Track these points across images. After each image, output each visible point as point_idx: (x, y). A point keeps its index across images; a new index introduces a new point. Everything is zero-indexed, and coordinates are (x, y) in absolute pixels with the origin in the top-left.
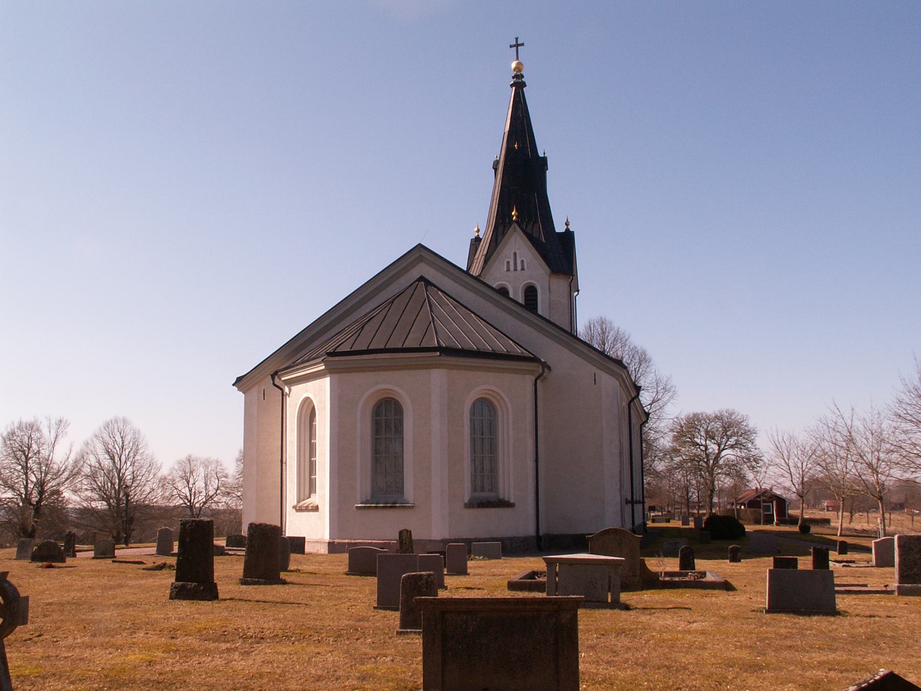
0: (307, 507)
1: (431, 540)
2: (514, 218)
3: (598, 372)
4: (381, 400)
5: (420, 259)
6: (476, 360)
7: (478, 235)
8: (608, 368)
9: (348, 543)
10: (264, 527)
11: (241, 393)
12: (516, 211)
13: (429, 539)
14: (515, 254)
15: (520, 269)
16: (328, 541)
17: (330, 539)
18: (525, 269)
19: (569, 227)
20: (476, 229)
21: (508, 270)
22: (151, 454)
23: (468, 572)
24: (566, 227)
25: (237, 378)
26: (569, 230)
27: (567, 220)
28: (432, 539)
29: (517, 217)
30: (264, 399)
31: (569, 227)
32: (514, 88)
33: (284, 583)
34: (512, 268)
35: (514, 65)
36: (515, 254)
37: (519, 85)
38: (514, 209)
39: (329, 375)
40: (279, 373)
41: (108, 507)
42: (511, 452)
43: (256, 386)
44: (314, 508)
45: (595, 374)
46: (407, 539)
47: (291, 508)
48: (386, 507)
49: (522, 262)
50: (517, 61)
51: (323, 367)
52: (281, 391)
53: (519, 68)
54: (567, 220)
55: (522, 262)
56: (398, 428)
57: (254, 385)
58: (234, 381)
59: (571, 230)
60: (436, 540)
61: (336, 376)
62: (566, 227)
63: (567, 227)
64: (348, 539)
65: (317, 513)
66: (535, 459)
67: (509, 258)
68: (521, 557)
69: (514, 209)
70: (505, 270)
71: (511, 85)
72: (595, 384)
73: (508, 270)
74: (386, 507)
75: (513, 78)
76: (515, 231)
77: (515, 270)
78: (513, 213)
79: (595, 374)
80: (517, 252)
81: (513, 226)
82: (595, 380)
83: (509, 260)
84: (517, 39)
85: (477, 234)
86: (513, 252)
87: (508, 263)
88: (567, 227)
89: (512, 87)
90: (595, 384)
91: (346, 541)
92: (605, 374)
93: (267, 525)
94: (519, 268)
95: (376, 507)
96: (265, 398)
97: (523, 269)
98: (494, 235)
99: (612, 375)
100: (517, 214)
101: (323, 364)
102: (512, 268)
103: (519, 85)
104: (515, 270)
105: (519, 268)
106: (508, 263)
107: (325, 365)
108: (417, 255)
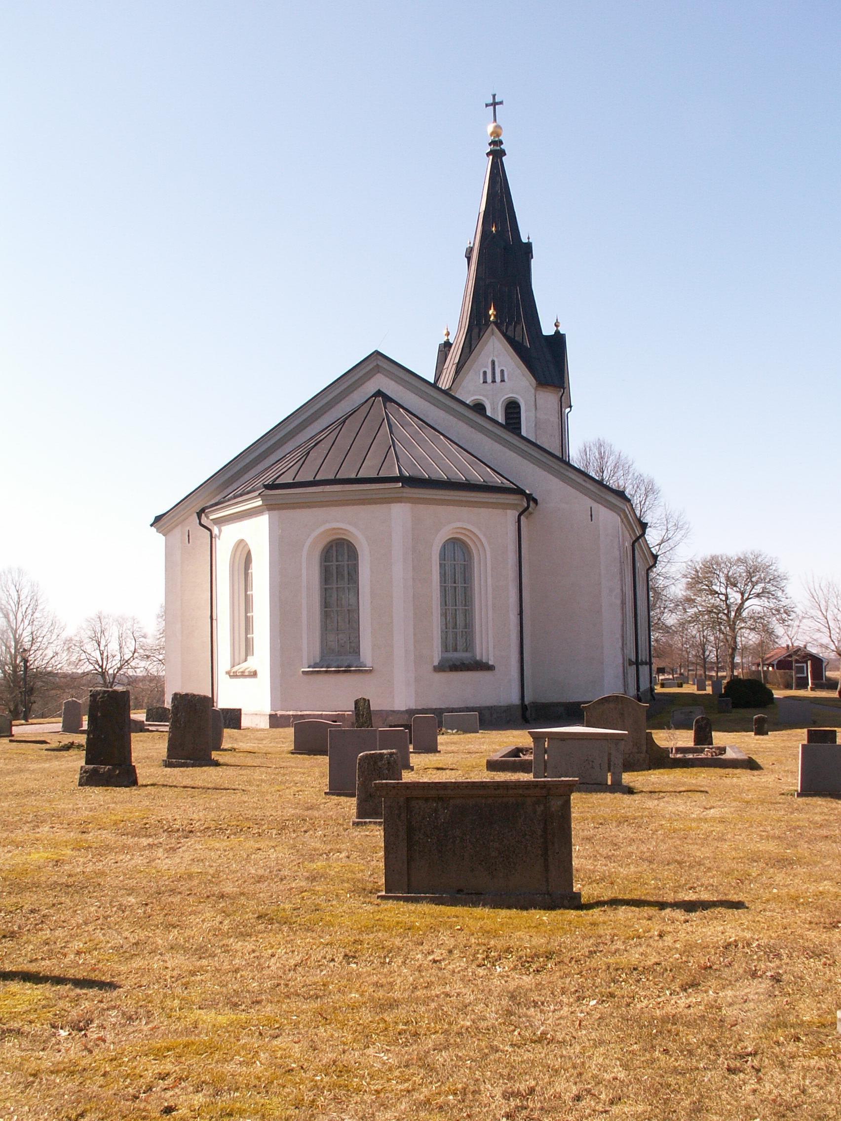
1: (394, 711)
3: (595, 506)
5: (377, 369)
6: (473, 494)
12: (494, 309)
14: (493, 363)
19: (559, 328)
20: (445, 332)
21: (485, 382)
24: (555, 328)
28: (395, 709)
31: (559, 328)
32: (491, 157)
34: (489, 379)
35: (490, 128)
36: (493, 363)
37: (497, 154)
42: (490, 603)
43: (179, 527)
49: (502, 371)
50: (495, 124)
51: (260, 503)
53: (496, 133)
55: (502, 371)
57: (177, 525)
61: (275, 513)
73: (485, 382)
75: (490, 144)
77: (494, 381)
78: (491, 312)
80: (495, 359)
82: (591, 516)
84: (494, 96)
87: (485, 373)
91: (291, 713)
92: (604, 508)
94: (498, 379)
95: (326, 672)
97: (503, 381)
102: (489, 379)
103: (497, 154)
104: (494, 381)
105: (498, 379)
106: (485, 373)
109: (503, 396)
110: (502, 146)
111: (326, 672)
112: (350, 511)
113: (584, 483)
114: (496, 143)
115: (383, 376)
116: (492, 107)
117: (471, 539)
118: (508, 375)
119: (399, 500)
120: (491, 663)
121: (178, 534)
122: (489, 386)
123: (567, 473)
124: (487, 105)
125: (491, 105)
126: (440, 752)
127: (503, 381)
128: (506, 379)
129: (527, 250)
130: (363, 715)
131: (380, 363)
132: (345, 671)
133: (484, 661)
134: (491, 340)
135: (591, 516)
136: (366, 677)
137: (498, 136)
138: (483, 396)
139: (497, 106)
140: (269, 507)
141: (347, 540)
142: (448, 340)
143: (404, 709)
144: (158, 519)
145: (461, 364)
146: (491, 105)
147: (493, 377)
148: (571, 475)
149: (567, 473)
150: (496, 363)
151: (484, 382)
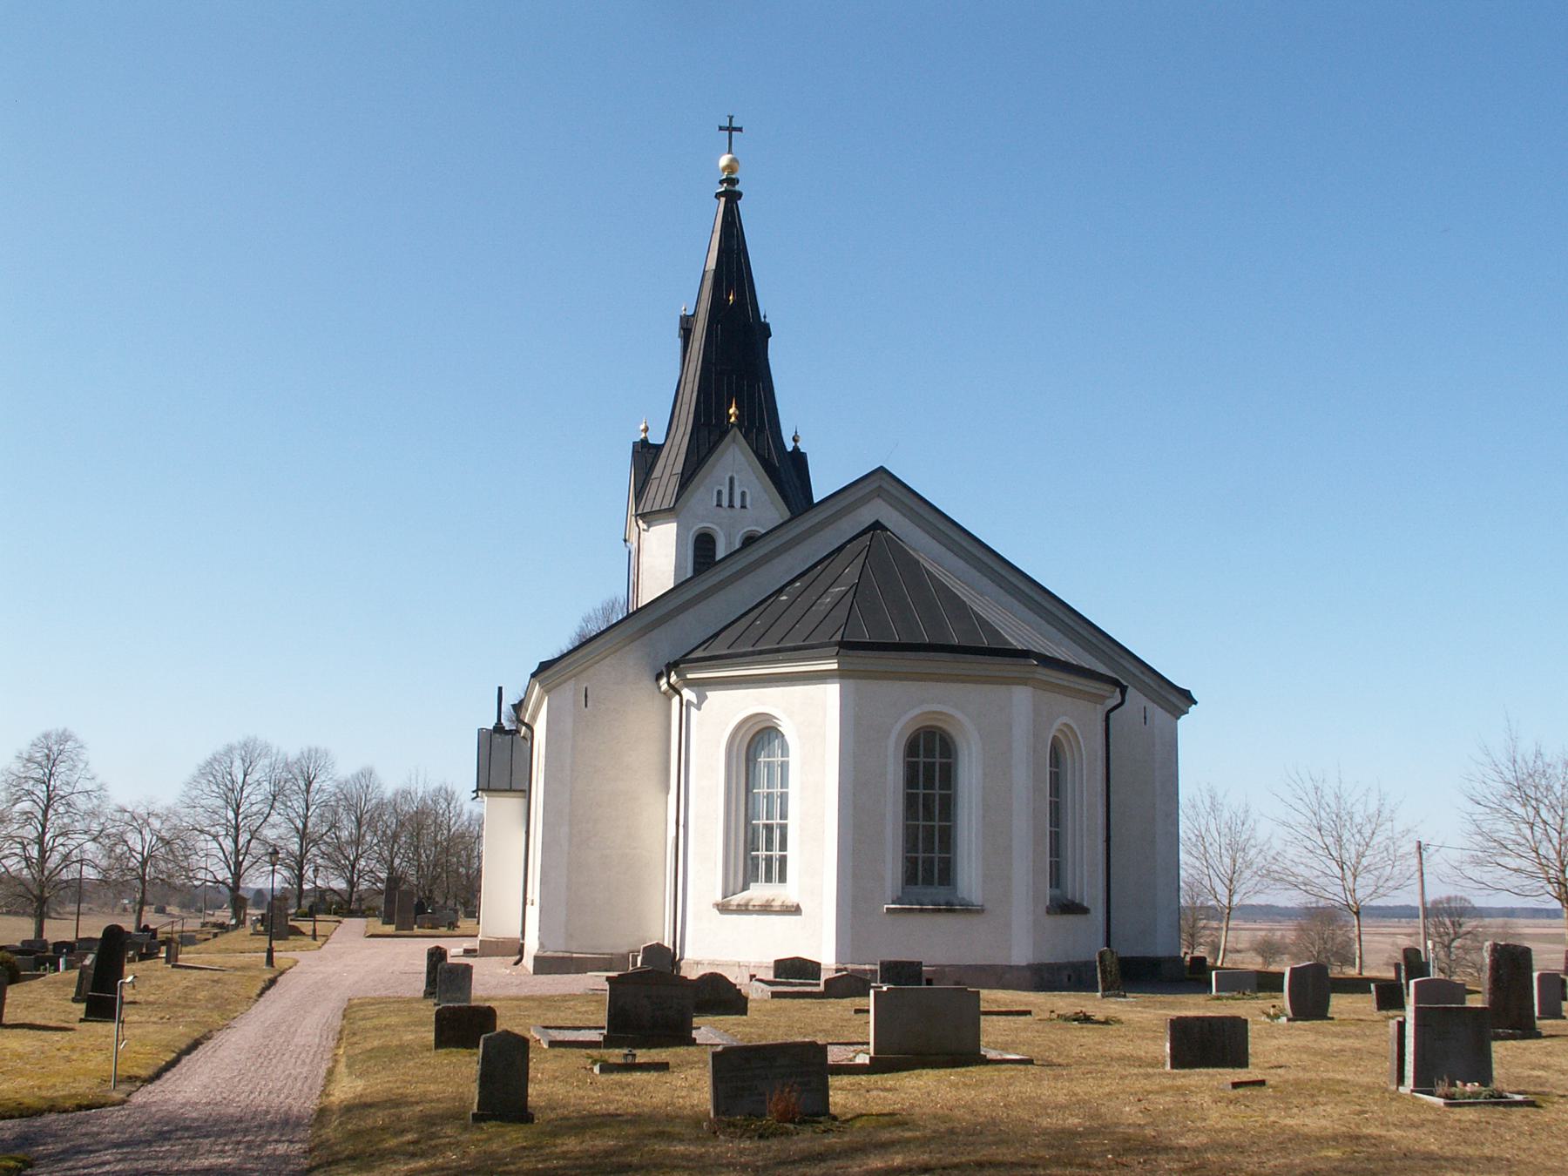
0: (747, 905)
1: (1011, 967)
2: (733, 419)
3: (1151, 706)
4: (921, 728)
5: (879, 492)
6: (1077, 679)
7: (646, 437)
8: (1168, 700)
9: (870, 970)
10: (1513, 949)
11: (1183, 717)
12: (736, 407)
13: (1008, 964)
14: (732, 480)
15: (727, 505)
16: (834, 967)
17: (836, 963)
18: (748, 506)
19: (798, 444)
20: (642, 427)
21: (719, 505)
22: (462, 801)
23: (1329, 1015)
24: (794, 444)
25: (541, 663)
26: (799, 450)
27: (796, 432)
28: (1012, 964)
29: (737, 417)
30: (586, 706)
31: (798, 444)
32: (723, 199)
33: (1539, 1036)
34: (725, 503)
35: (724, 160)
36: (732, 480)
37: (731, 197)
38: (734, 405)
39: (838, 680)
40: (681, 666)
41: (1199, 905)
43: (572, 682)
44: (793, 909)
45: (1145, 708)
46: (1113, 965)
47: (1092, 911)
48: (940, 910)
49: (743, 494)
50: (730, 156)
51: (835, 666)
52: (1111, 714)
53: (731, 167)
54: (796, 432)
55: (743, 494)
56: (948, 776)
57: (570, 678)
58: (534, 669)
59: (802, 451)
60: (1018, 966)
62: (794, 444)
63: (796, 445)
64: (869, 964)
65: (798, 917)
66: (1105, 839)
67: (721, 485)
68: (1152, 993)
69: (734, 405)
70: (715, 504)
71: (717, 193)
72: (1145, 723)
73: (719, 505)
74: (940, 910)
75: (721, 182)
76: (734, 441)
77: (731, 506)
78: (731, 411)
79: (1145, 708)
80: (736, 477)
81: (732, 433)
82: (1145, 718)
83: (721, 488)
84: (731, 118)
85: (643, 435)
86: (730, 474)
87: (719, 493)
88: (796, 445)
89: (719, 199)
90: (1145, 723)
91: (867, 967)
92: (1160, 709)
93: (1516, 946)
94: (737, 503)
95: (921, 910)
96: (588, 705)
97: (743, 507)
98: (692, 442)
99: (1169, 712)
100: (737, 412)
101: (836, 661)
102: (725, 503)
103: (731, 197)
104: (731, 506)
105: (737, 503)
106: (719, 493)
107: (838, 663)
108: (876, 485)
109: (743, 528)
110: (737, 187)
111: (921, 910)
112: (956, 689)
113: (1140, 675)
114: (731, 181)
115: (883, 503)
116: (727, 132)
117: (1069, 741)
118: (752, 499)
119: (1023, 681)
120: (1085, 904)
121: (569, 691)
122: (724, 512)
123: (1121, 661)
124: (721, 128)
125: (727, 129)
126: (1332, 1019)
127: (743, 507)
128: (748, 504)
129: (765, 331)
130: (1111, 971)
131: (885, 486)
132: (948, 911)
133: (1077, 901)
134: (731, 449)
135: (1145, 718)
136: (974, 920)
137: (732, 172)
138: (717, 525)
139: (734, 133)
140: (839, 675)
141: (940, 728)
142: (646, 437)
143: (1024, 963)
144: (544, 667)
145: (686, 476)
146: (727, 129)
147: (729, 501)
148: (1125, 663)
149: (1121, 661)
150: (736, 483)
151: (717, 505)
